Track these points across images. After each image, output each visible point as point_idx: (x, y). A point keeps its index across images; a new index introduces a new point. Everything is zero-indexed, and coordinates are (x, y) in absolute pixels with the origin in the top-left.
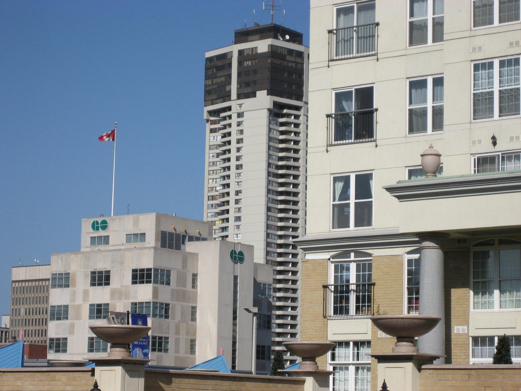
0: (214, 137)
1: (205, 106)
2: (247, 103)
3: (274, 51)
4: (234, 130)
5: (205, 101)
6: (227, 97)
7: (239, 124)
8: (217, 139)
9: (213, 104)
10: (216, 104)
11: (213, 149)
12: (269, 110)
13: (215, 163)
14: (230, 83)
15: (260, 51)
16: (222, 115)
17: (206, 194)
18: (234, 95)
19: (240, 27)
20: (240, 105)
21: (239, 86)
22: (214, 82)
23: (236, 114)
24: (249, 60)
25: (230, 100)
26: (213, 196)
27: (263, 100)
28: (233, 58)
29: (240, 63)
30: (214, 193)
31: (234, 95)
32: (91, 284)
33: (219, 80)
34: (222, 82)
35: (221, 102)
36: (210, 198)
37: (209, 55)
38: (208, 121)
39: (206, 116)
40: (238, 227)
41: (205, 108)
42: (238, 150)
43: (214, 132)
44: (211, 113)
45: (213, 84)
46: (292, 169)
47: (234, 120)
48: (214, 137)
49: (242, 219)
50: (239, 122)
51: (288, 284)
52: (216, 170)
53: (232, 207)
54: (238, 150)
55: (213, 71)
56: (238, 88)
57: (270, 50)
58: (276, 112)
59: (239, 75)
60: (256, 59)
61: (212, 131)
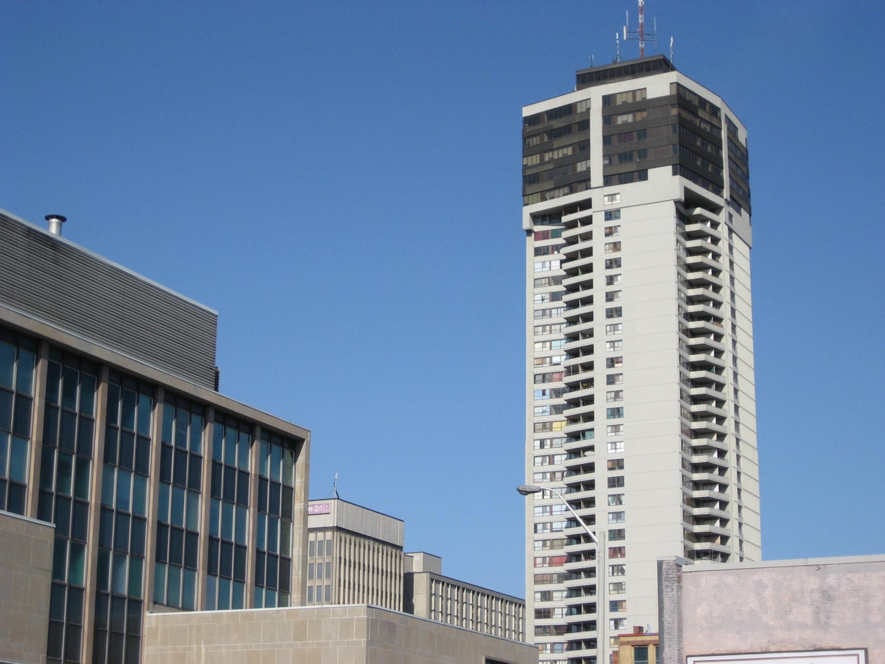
0: (544, 263)
1: (526, 205)
2: (627, 193)
3: (682, 98)
4: (599, 243)
5: (524, 195)
6: (584, 181)
7: (610, 232)
8: (553, 265)
9: (544, 199)
10: (552, 198)
11: (542, 285)
12: (677, 202)
13: (548, 312)
14: (587, 158)
15: (650, 95)
16: (566, 219)
17: (531, 370)
18: (597, 178)
19: (585, 67)
20: (612, 196)
21: (607, 162)
22: (547, 159)
23: (603, 213)
24: (629, 113)
25: (588, 188)
26: (544, 375)
27: (665, 184)
28: (591, 110)
29: (607, 120)
30: (547, 369)
31: (597, 178)
32: (619, 416)
33: (557, 155)
34: (566, 157)
35: (565, 195)
36: (540, 378)
37: (529, 111)
38: (529, 232)
39: (527, 223)
40: (616, 428)
41: (525, 208)
42: (610, 280)
43: (544, 254)
44: (538, 218)
45: (542, 163)
46: (712, 321)
47: (599, 225)
48: (544, 263)
49: (625, 412)
50: (611, 228)
51: (713, 541)
52: (551, 325)
53: (600, 390)
54: (610, 280)
55: (542, 139)
56: (605, 166)
57: (675, 92)
58: (686, 208)
59: (606, 140)
60: (644, 110)
61: (538, 252)
